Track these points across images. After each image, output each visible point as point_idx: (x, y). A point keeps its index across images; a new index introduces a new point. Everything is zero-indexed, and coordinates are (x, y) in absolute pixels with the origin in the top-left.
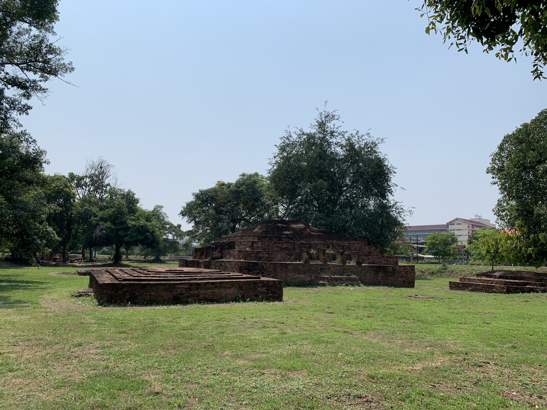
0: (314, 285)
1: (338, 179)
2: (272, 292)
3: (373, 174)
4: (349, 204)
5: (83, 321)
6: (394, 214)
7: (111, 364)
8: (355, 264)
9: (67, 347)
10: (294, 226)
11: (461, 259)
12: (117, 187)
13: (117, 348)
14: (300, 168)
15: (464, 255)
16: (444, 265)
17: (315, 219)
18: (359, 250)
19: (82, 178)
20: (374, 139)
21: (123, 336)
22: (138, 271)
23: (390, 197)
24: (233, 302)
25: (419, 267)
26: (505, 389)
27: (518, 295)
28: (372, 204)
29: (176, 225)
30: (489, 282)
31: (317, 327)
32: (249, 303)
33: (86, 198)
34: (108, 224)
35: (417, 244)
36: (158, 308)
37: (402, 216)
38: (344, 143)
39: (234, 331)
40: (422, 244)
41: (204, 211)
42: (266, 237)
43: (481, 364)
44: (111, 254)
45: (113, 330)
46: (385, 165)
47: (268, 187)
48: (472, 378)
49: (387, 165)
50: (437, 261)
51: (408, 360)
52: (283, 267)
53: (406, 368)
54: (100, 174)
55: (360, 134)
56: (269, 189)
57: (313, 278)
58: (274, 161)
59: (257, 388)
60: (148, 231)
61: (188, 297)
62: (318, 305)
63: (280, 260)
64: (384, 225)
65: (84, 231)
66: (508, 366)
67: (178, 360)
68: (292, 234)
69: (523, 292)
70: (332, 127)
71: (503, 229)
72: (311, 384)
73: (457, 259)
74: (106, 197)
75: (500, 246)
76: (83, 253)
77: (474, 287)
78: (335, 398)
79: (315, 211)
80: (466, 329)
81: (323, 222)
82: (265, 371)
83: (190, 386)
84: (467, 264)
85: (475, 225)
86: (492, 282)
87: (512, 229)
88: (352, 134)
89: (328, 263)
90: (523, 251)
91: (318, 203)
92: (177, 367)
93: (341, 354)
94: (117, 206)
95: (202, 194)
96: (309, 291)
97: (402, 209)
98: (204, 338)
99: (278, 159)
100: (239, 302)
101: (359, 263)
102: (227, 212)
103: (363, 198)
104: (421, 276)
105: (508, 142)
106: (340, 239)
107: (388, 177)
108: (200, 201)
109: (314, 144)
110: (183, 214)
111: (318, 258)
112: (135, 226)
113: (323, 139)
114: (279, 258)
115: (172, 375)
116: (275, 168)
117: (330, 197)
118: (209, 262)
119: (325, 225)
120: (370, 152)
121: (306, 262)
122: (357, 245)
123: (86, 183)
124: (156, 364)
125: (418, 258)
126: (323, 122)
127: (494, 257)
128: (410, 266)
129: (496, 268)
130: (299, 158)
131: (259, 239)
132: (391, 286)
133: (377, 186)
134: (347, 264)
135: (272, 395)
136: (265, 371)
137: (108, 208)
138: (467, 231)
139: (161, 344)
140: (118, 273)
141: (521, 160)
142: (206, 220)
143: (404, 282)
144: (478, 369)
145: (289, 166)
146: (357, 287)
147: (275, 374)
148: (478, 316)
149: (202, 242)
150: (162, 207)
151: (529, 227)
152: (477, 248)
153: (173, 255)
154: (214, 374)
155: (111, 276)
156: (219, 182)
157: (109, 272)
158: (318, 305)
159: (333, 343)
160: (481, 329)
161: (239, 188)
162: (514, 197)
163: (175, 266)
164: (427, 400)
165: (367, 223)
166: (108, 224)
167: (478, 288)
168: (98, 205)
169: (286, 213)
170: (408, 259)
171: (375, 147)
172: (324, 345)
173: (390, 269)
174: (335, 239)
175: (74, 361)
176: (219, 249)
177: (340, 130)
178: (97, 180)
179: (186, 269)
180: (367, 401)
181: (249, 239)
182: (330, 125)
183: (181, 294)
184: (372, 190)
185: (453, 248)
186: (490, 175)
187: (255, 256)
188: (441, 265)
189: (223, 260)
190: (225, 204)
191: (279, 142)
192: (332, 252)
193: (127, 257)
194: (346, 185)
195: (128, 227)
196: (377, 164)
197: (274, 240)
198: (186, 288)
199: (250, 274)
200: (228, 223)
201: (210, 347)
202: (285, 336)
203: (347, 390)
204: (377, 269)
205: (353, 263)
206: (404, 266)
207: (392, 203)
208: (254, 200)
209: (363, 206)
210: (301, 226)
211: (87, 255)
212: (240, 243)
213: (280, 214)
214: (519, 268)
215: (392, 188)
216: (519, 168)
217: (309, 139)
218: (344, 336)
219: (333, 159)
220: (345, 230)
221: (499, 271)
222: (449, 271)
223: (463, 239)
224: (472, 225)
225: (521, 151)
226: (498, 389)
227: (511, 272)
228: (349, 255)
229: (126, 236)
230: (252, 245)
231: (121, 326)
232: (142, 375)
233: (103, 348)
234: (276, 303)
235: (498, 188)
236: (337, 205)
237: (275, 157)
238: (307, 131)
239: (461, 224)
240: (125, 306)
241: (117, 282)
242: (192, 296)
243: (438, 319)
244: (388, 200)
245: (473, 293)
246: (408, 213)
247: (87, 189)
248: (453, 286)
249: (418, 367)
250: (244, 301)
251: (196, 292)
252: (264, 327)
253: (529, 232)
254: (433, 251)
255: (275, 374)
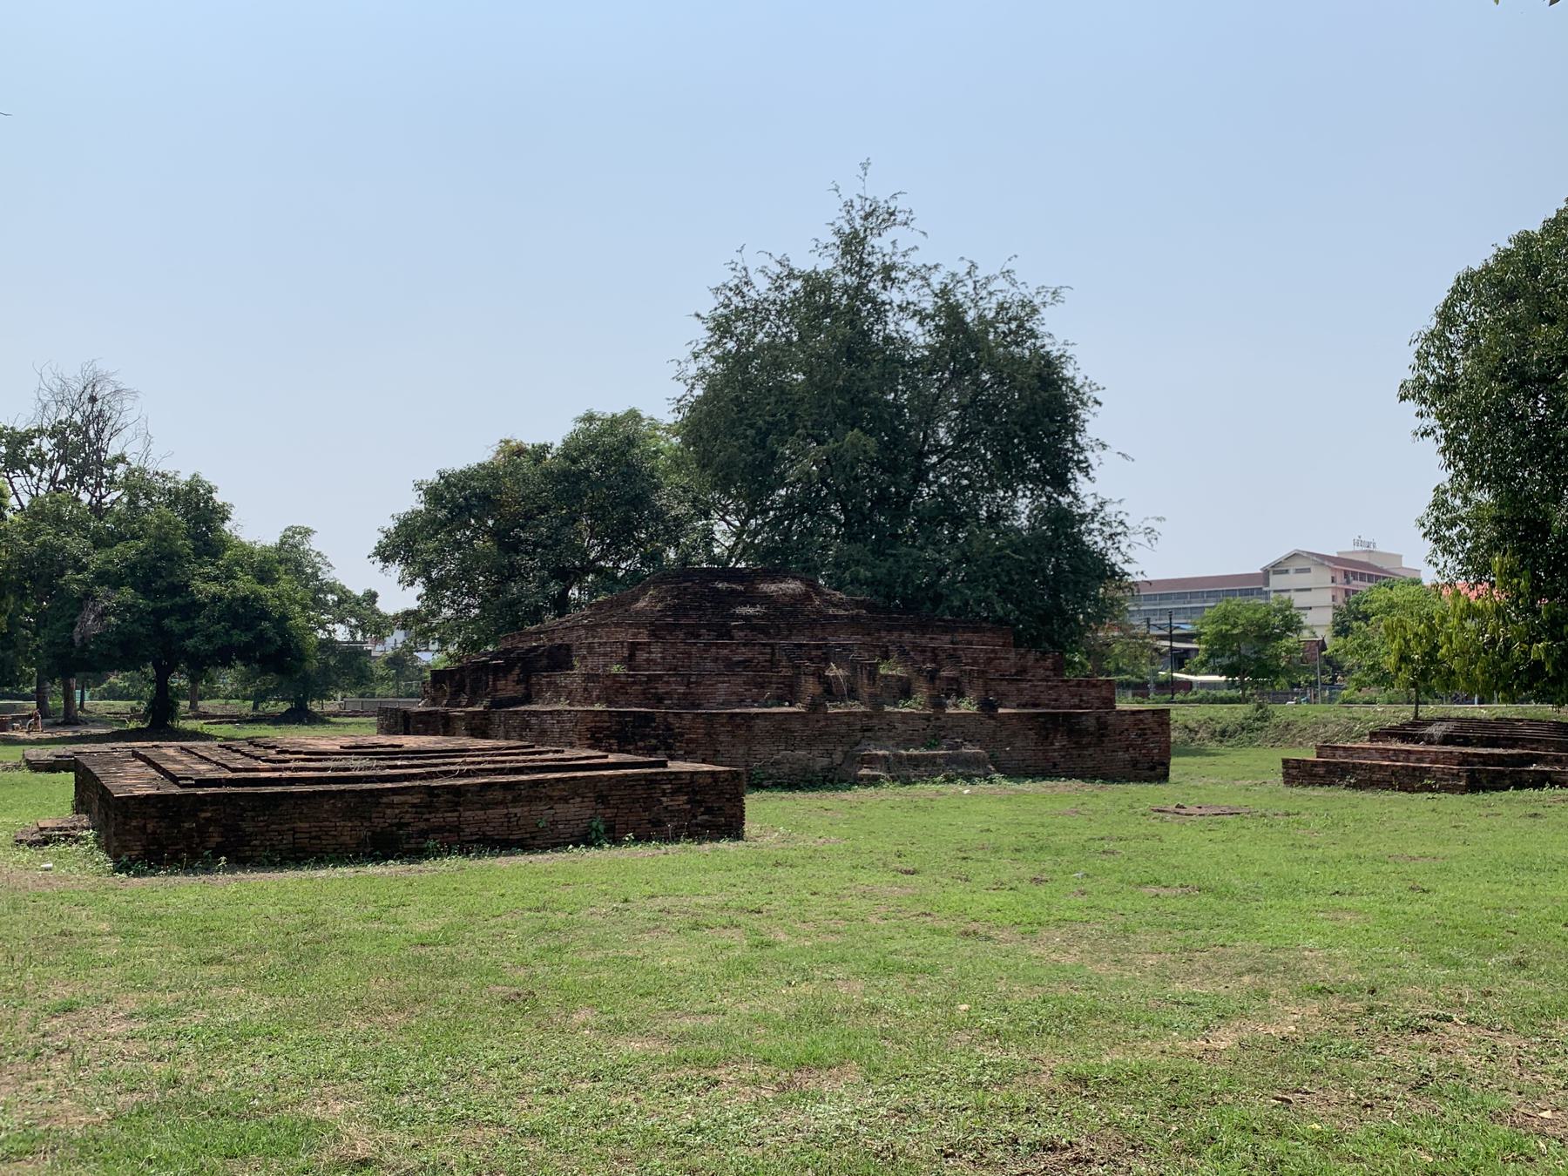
0: (841, 781)
1: (910, 425)
2: (709, 811)
3: (1031, 414)
4: (948, 512)
5: (64, 925)
6: (1095, 540)
7: (188, 1071)
8: (974, 709)
9: (25, 1016)
10: (770, 588)
11: (1312, 684)
12: (151, 467)
13: (200, 1016)
14: (783, 392)
15: (1322, 672)
16: (1260, 707)
17: (837, 565)
18: (990, 660)
19: (27, 438)
20: (1028, 292)
21: (216, 971)
22: (246, 749)
23: (1082, 485)
24: (576, 846)
25: (1182, 714)
26: (1512, 1099)
27: (1506, 795)
28: (1023, 507)
29: (359, 593)
30: (1413, 758)
31: (873, 920)
32: (633, 848)
33: (43, 506)
34: (127, 594)
35: (1171, 638)
36: (323, 873)
37: (1123, 548)
38: (928, 304)
39: (596, 945)
40: (1187, 638)
41: (458, 545)
42: (676, 626)
43: (1424, 1022)
44: (139, 698)
45: (178, 954)
46: (1065, 380)
47: (675, 459)
48: (1403, 1069)
49: (1072, 380)
50: (1233, 693)
51: (1187, 1018)
52: (738, 726)
53: (1184, 1046)
54: (88, 421)
55: (980, 274)
56: (678, 464)
57: (838, 757)
58: (693, 369)
59: (701, 1131)
60: (264, 615)
61: (424, 834)
62: (865, 847)
63: (727, 704)
64: (1063, 579)
65: (42, 619)
66: (1510, 1025)
67: (419, 1049)
68: (764, 616)
69: (1520, 786)
70: (888, 249)
71: (1451, 584)
72: (882, 1111)
73: (1298, 685)
74: (113, 503)
75: (1442, 639)
76: (40, 697)
77: (1362, 775)
78: (971, 1156)
79: (836, 537)
80: (1359, 912)
81: (864, 573)
82: (720, 1073)
83: (470, 1132)
84: (1331, 700)
85: (1354, 574)
86: (1421, 756)
87: (1479, 582)
88: (954, 275)
89: (888, 709)
90: (1516, 653)
91: (844, 509)
92: (419, 1070)
93: (965, 1007)
94: (152, 531)
95: (448, 485)
96: (826, 804)
97: (1121, 523)
98: (496, 970)
99: (707, 362)
100: (600, 846)
101: (988, 707)
102: (536, 545)
103: (993, 489)
104: (1185, 743)
105: (1469, 294)
106: (923, 627)
107: (1076, 417)
108: (445, 512)
109: (828, 309)
110: (385, 554)
111: (852, 694)
112: (221, 599)
113: (857, 292)
114: (721, 697)
115: (406, 1099)
116: (699, 392)
117: (883, 492)
118: (484, 715)
119: (872, 583)
120: (1016, 333)
121: (815, 707)
122: (979, 646)
123: (39, 453)
124: (345, 1064)
125: (1171, 686)
126: (856, 232)
127: (1424, 675)
128: (1154, 712)
129: (1429, 710)
130: (776, 357)
131: (653, 634)
132: (1093, 778)
133: (1042, 451)
134: (950, 711)
135: (758, 1151)
136: (720, 1073)
137: (122, 538)
138: (1329, 594)
139: (351, 997)
140: (180, 762)
141: (1511, 356)
142: (466, 573)
143: (1135, 763)
144: (1418, 1039)
145: (747, 384)
146: (982, 786)
147: (756, 1082)
148: (1391, 868)
149: (452, 649)
150: (307, 532)
151: (1534, 576)
152: (1368, 647)
153: (352, 696)
154: (550, 1091)
155: (153, 772)
156: (507, 442)
157: (143, 758)
158: (865, 847)
159: (932, 970)
160: (1408, 909)
161: (574, 461)
162: (1486, 479)
163: (364, 731)
164: (1272, 1147)
165: (1008, 573)
166: (127, 594)
167: (1376, 777)
168: (87, 529)
169: (736, 544)
170: (1140, 689)
171: (1030, 316)
172: (904, 978)
173: (1091, 723)
174: (905, 628)
175: (56, 1065)
176: (517, 671)
177: (916, 260)
178: (81, 445)
179: (410, 742)
180: (1077, 1160)
181: (621, 637)
182: (881, 245)
183: (400, 826)
184: (1024, 463)
185: (1288, 651)
186: (1412, 406)
187: (644, 693)
188: (1252, 706)
189: (533, 707)
190: (529, 517)
191: (709, 305)
192: (899, 671)
193: (193, 707)
194: (939, 449)
195: (194, 602)
196: (1039, 376)
197: (706, 636)
198: (414, 805)
199: (629, 752)
200: (544, 584)
201: (521, 1001)
202: (769, 952)
203: (1008, 1126)
204: (1050, 725)
205: (968, 706)
206: (1134, 713)
207: (1090, 504)
208: (628, 502)
209: (994, 519)
210: (793, 586)
211: (56, 702)
212: (590, 647)
213: (717, 551)
214: (1498, 709)
215: (1088, 454)
216: (1504, 380)
217: (813, 293)
218: (966, 948)
219: (892, 361)
220: (938, 599)
221: (1442, 720)
222: (1276, 726)
223: (1318, 622)
224: (1346, 574)
225: (1512, 324)
226: (1494, 1104)
227: (1483, 724)
228: (955, 680)
229: (190, 633)
230: (632, 656)
231: (205, 939)
232: (299, 1103)
233: (151, 1016)
234: (724, 845)
235: (1437, 447)
236: (909, 515)
237: (696, 356)
238: (806, 262)
239: (1308, 570)
240: (207, 870)
241: (176, 790)
242: (439, 830)
243: (1263, 883)
244: (1076, 496)
245: (1360, 794)
246: (1142, 539)
247: (46, 475)
248: (1294, 772)
249: (1225, 1040)
250: (616, 841)
251: (451, 817)
252: (696, 927)
253: (1537, 590)
254: (1225, 661)
255: (756, 1082)
